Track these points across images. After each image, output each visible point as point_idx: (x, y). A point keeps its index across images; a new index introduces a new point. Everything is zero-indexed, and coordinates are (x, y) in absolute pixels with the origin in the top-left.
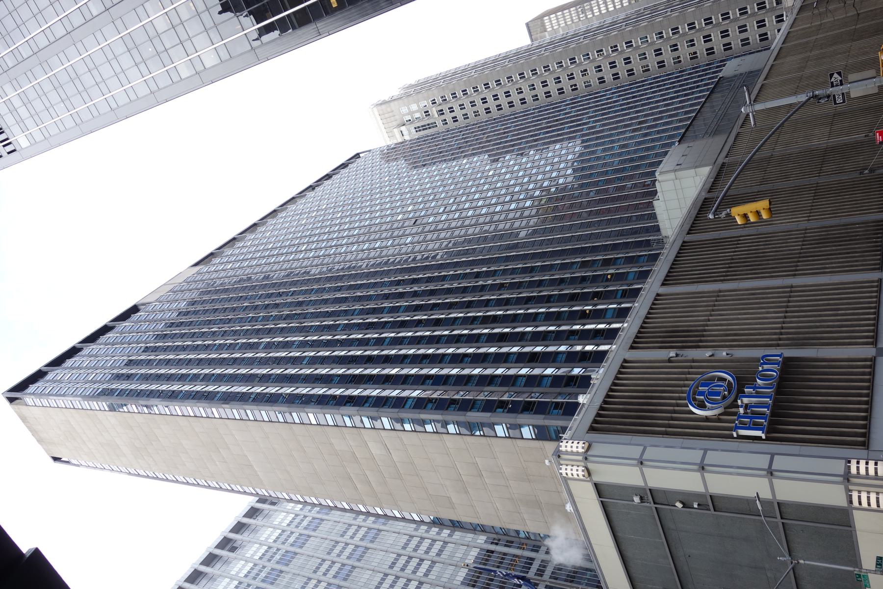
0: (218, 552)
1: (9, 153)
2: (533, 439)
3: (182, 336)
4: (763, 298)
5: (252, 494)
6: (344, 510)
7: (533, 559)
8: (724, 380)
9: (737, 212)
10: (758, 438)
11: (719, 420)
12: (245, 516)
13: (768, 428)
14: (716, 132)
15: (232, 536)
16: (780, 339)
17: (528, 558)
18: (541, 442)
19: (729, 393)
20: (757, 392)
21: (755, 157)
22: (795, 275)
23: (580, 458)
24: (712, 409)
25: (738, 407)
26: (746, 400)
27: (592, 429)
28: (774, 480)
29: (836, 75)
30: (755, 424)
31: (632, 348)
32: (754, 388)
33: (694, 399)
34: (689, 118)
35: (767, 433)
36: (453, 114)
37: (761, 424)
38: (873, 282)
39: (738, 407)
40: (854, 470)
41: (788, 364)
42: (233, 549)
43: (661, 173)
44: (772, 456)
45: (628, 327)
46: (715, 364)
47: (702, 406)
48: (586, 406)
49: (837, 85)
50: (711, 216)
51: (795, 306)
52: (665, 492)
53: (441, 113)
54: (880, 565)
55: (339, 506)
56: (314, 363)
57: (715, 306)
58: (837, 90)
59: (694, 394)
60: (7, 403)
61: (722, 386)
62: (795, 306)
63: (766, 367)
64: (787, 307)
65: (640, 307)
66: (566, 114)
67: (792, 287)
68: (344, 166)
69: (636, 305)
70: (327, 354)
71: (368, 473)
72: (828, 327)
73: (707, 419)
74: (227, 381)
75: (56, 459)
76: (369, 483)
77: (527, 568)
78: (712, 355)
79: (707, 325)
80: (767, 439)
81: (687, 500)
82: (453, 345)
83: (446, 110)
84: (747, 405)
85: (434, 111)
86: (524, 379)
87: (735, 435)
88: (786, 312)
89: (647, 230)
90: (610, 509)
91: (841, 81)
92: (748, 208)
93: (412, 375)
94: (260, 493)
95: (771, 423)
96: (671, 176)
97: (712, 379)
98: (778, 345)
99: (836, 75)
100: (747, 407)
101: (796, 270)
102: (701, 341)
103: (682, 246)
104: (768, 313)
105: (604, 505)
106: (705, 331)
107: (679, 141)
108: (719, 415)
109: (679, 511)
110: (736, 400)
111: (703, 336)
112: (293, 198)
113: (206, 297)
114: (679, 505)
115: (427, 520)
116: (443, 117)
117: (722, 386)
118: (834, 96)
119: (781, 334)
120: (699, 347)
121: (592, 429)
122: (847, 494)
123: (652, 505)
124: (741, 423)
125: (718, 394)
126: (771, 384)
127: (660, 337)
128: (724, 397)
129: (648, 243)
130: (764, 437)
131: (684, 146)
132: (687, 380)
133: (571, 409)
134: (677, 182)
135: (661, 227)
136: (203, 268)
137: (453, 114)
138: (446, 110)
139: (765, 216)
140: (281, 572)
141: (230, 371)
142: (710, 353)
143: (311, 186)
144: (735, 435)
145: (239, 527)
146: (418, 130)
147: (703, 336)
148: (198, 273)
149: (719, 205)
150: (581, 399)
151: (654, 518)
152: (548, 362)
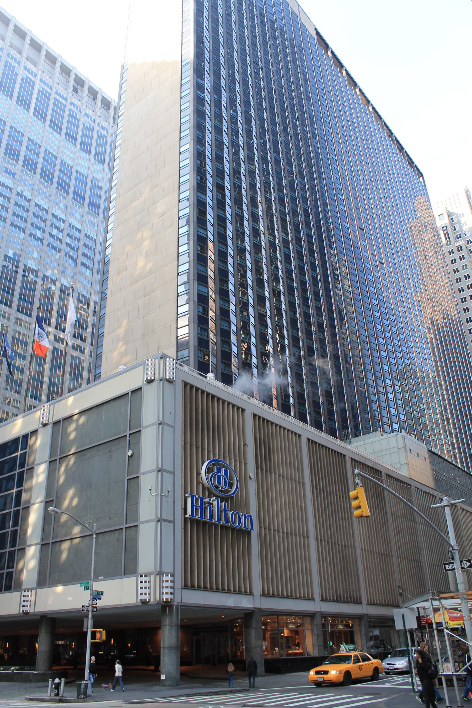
0: (72, 77)
2: (177, 337)
3: (253, 27)
4: (298, 517)
5: (119, 101)
6: (111, 182)
7: (10, 306)
9: (360, 492)
11: (198, 483)
12: (103, 97)
13: (194, 519)
14: (437, 480)
15: (86, 88)
16: (265, 529)
17: (11, 302)
18: (468, 638)
19: (221, 491)
20: (222, 511)
21: (416, 514)
22: (317, 540)
26: (215, 503)
27: (185, 384)
29: (468, 564)
31: (255, 415)
32: (225, 509)
33: (214, 465)
34: (457, 462)
35: (190, 519)
36: (458, 260)
38: (312, 595)
39: (210, 497)
40: (165, 578)
41: (249, 533)
42: (75, 90)
43: (403, 437)
44: (173, 522)
46: (244, 479)
47: (209, 470)
48: (204, 379)
49: (461, 565)
50: (356, 471)
51: (292, 539)
52: (139, 442)
53: (460, 249)
54: (98, 593)
55: (114, 177)
56: (233, 146)
57: (292, 480)
58: (457, 565)
59: (218, 464)
61: (226, 485)
62: (292, 539)
63: (243, 518)
64: (291, 534)
66: (457, 357)
67: (308, 537)
68: (411, 162)
69: (293, 419)
70: (242, 157)
72: (276, 563)
73: (199, 474)
74: (213, 37)
77: (78, 336)
78: (251, 478)
79: (275, 474)
80: (185, 519)
82: (254, 267)
83: (461, 254)
84: (212, 504)
85: (461, 242)
86: (227, 328)
87: (186, 495)
88: (287, 533)
89: (356, 427)
90: (123, 399)
91: (464, 568)
92: (363, 500)
93: (226, 232)
94: (121, 108)
95: (198, 522)
96: (401, 445)
97: (231, 479)
98: (260, 527)
99: (468, 564)
100: (210, 504)
101: (321, 540)
102: (262, 470)
103: (341, 454)
104: (286, 520)
106: (271, 473)
107: (430, 451)
108: (203, 484)
109: (125, 453)
110: (215, 496)
111: (266, 471)
112: (381, 118)
113: (287, 44)
114: (130, 453)
115: (108, 252)
116: (455, 251)
117: (226, 485)
118: (453, 563)
119: (270, 530)
120: (257, 468)
121: (185, 384)
122: (148, 573)
123: (128, 433)
124: (197, 499)
125: (219, 482)
126: (229, 522)
127: (264, 438)
128: (217, 487)
129: (345, 427)
130: (187, 516)
131: (426, 454)
132: (230, 459)
133: (203, 368)
134: (396, 450)
135: (358, 438)
136: (314, 35)
137: (458, 260)
138: (461, 254)
139: (356, 513)
140: (92, 182)
141: (223, 72)
142: (252, 477)
143: (392, 133)
144: (186, 495)
145: (93, 93)
146: (445, 228)
147: (266, 471)
148: (311, 36)
149: (365, 477)
150: (211, 376)
151: (117, 435)
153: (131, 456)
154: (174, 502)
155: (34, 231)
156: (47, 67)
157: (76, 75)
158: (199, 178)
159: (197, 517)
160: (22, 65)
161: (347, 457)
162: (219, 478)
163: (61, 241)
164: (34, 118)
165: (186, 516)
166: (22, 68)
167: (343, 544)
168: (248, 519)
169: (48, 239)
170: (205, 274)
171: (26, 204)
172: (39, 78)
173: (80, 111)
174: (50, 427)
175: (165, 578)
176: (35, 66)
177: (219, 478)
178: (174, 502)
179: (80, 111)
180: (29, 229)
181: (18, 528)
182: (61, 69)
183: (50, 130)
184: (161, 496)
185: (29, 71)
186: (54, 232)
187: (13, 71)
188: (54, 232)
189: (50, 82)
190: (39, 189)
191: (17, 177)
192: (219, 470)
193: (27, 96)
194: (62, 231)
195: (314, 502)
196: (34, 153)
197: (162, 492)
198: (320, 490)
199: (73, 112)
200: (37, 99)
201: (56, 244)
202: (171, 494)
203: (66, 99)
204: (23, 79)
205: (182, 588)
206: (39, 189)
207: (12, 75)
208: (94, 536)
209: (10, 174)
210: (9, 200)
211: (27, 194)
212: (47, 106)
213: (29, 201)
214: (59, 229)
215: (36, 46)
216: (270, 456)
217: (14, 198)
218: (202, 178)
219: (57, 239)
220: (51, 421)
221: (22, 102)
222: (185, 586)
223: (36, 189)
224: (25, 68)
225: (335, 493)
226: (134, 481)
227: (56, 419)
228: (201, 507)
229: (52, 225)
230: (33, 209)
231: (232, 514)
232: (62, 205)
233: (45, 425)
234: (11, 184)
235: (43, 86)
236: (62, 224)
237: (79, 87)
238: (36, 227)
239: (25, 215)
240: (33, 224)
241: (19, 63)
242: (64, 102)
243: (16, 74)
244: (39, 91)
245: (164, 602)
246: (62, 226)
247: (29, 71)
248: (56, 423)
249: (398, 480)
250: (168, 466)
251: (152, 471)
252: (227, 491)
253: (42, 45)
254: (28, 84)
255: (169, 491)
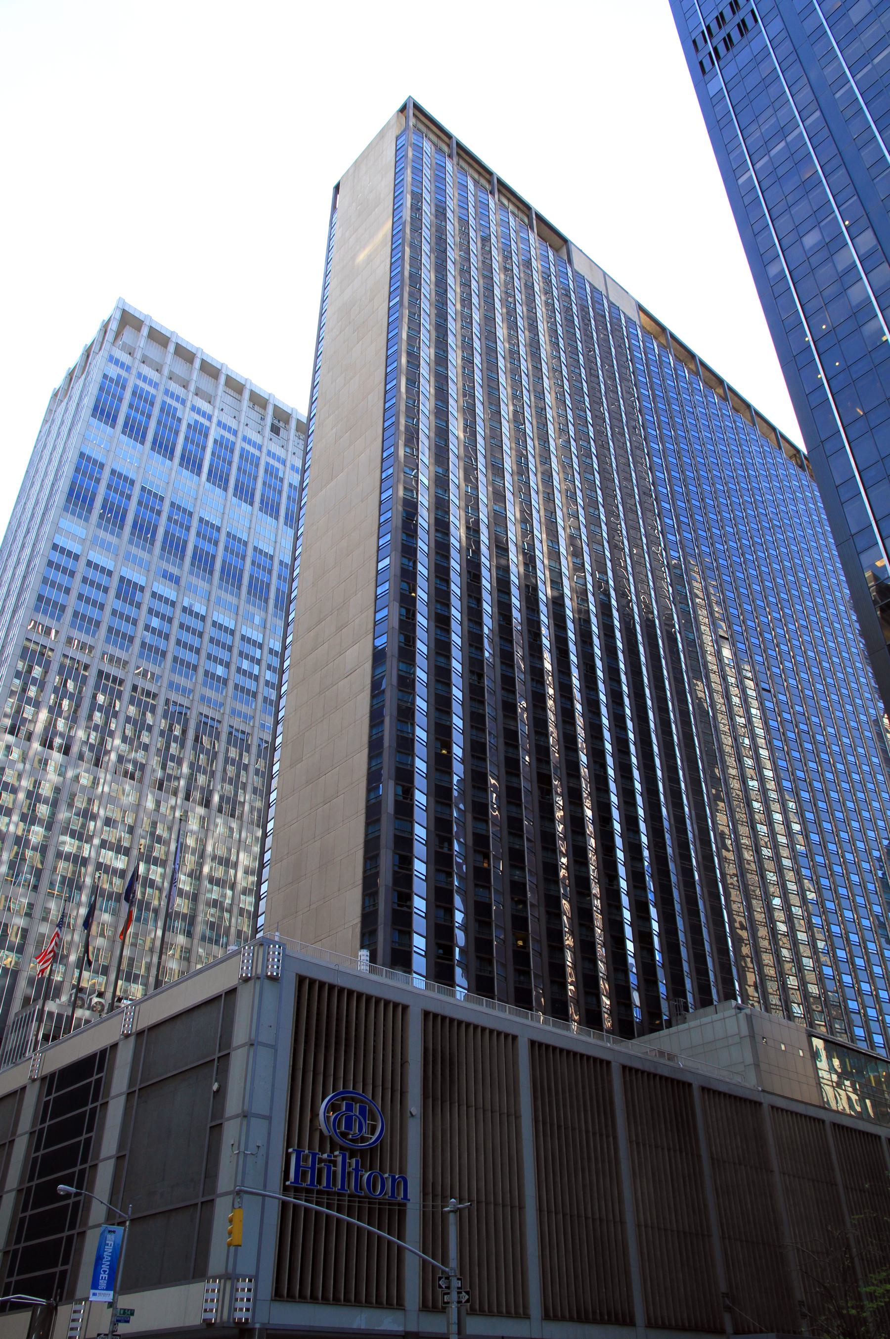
1: (701, 63)
8: (373, 1133)
10: (286, 1177)
19: (351, 1140)
23: (259, 971)
24: (327, 1119)
25: (332, 1151)
26: (340, 1159)
28: (231, 1197)
30: (304, 1173)
31: (426, 1014)
32: (357, 1170)
37: (304, 1179)
42: (275, 430)
45: (460, 997)
60: (399, 106)
61: (360, 1129)
65: (498, 1015)
71: (326, 645)
73: (315, 1115)
75: (337, 188)
76: (315, 649)
81: (220, 1095)
87: (290, 1150)
97: (374, 1119)
102: (434, 1100)
105: (217, 998)
109: (211, 1085)
110: (342, 1149)
114: (215, 1087)
117: (360, 1129)
125: (349, 1126)
128: (344, 1135)
134: (737, 1039)
152: (624, 796)
153: (218, 1090)
154: (267, 1163)
155: (211, 666)
156: (229, 400)
157: (275, 407)
158: (404, 611)
159: (304, 1185)
160: (189, 404)
161: (613, 1064)
162: (349, 1120)
163: (257, 678)
164: (208, 485)
165: (288, 1183)
166: (188, 409)
167: (597, 1216)
168: (399, 1183)
169: (235, 678)
170: (409, 768)
171: (197, 624)
172: (215, 420)
173: (284, 463)
174: (132, 1039)
175: (240, 1285)
176: (210, 402)
177: (349, 1120)
178: (267, 1163)
179: (284, 463)
180: (204, 664)
181: (93, 1134)
182: (251, 399)
183: (235, 500)
184: (245, 1155)
185: (199, 412)
186: (246, 665)
187: (174, 416)
188: (246, 665)
189: (233, 424)
190: (219, 599)
191: (183, 583)
192: (349, 1108)
193: (196, 451)
194: (259, 662)
195: (629, 1131)
196: (210, 541)
197: (246, 1149)
198: (552, 1125)
199: (273, 466)
200: (213, 454)
201: (250, 685)
202: (263, 1151)
203: (260, 448)
204: (189, 426)
205: (272, 1300)
206: (219, 599)
207: (172, 424)
208: (128, 1223)
209: (171, 580)
210: (170, 620)
211: (200, 608)
212: (230, 463)
213: (203, 619)
214: (252, 659)
215: (210, 370)
216: (451, 1075)
217: (178, 615)
218: (408, 611)
219: (250, 675)
220: (134, 1031)
221: (188, 463)
222: (277, 1295)
223: (213, 598)
224: (193, 408)
225: (584, 1128)
226: (216, 1129)
227: (140, 1027)
228: (313, 1168)
229: (241, 654)
230: (210, 631)
231: (369, 1176)
232: (257, 620)
233: (127, 1036)
234: (172, 596)
235: (222, 432)
236: (258, 651)
237: (282, 424)
238: (215, 659)
239: (196, 642)
240: (209, 657)
241: (183, 402)
242: (257, 453)
243: (179, 420)
244: (216, 441)
245: (234, 1322)
246: (258, 654)
247: (199, 412)
248: (140, 1034)
249: (730, 1096)
250: (260, 1107)
251: (237, 1116)
252: (363, 1139)
253: (219, 367)
254: (198, 431)
255: (258, 1147)
